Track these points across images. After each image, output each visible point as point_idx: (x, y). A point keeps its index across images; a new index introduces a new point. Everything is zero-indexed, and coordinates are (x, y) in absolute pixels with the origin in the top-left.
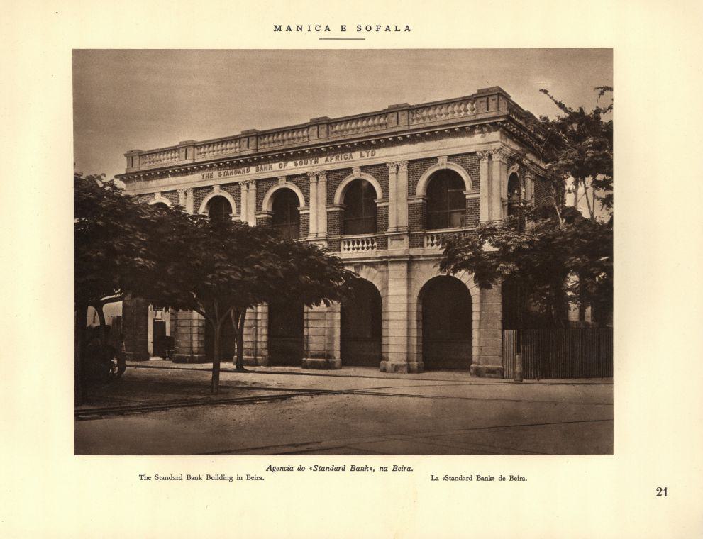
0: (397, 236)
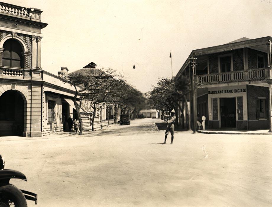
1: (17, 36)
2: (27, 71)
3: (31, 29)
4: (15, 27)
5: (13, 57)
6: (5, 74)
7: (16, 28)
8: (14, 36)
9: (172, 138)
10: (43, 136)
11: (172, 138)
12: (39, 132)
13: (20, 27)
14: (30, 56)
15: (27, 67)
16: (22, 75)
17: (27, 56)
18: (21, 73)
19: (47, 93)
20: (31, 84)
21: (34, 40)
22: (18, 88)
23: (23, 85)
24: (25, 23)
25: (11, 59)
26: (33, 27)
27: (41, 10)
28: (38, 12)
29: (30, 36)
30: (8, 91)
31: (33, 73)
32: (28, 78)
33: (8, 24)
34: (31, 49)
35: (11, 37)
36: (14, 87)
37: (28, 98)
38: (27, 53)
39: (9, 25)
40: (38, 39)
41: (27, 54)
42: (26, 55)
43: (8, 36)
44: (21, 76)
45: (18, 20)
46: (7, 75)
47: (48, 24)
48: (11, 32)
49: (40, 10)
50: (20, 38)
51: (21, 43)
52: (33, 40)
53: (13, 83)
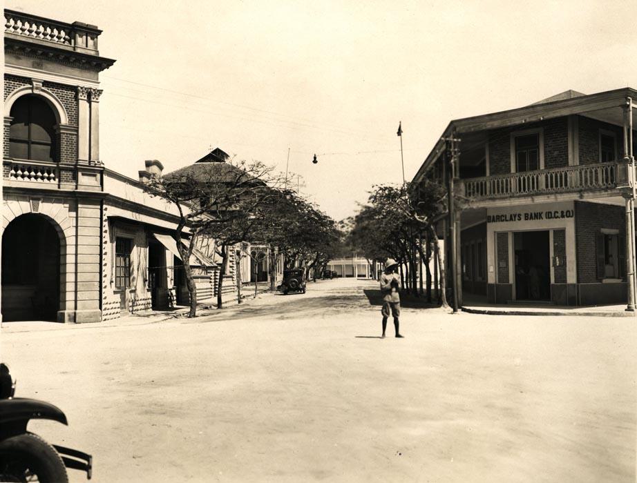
1: (43, 88)
3: (76, 72)
4: (38, 66)
6: (16, 176)
8: (37, 88)
14: (73, 135)
15: (65, 161)
17: (67, 134)
18: (52, 175)
20: (75, 200)
22: (46, 209)
23: (58, 201)
24: (62, 57)
25: (29, 142)
27: (99, 29)
30: (23, 215)
32: (68, 187)
34: (75, 118)
35: (30, 91)
36: (36, 207)
37: (69, 233)
40: (93, 96)
43: (22, 87)
46: (19, 178)
47: (115, 61)
49: (97, 27)
53: (35, 196)
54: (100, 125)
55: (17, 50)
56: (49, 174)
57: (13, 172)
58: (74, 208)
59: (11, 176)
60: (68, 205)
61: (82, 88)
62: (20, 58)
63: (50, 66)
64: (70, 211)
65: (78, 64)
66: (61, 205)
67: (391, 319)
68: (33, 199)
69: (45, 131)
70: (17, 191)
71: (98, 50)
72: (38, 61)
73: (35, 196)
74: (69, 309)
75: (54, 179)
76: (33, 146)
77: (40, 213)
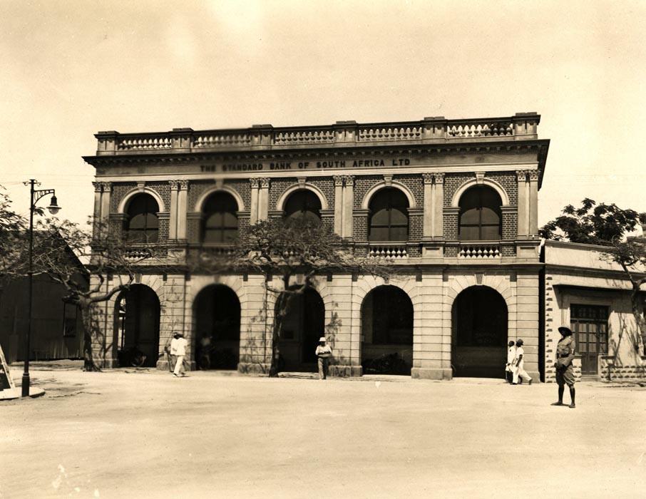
0: (434, 245)
1: (486, 178)
2: (508, 245)
3: (515, 158)
4: (480, 161)
5: (485, 221)
6: (466, 255)
7: (143, 173)
8: (480, 179)
9: (573, 393)
10: (549, 382)
11: (573, 393)
12: (533, 372)
13: (448, 159)
14: (514, 214)
15: (507, 238)
16: (405, 255)
17: (508, 214)
18: (497, 251)
19: (560, 289)
20: (515, 271)
21: (522, 179)
22: (489, 281)
23: (500, 274)
24: (509, 148)
25: (480, 225)
26: (517, 153)
27: (538, 114)
28: (534, 119)
29: (513, 173)
30: (469, 288)
31: (518, 248)
32: (509, 261)
33: (465, 159)
34: (514, 199)
35: (475, 183)
36: (479, 280)
37: (510, 301)
38: (507, 209)
39: (469, 159)
40: (182, 186)
41: (415, 212)
42: (505, 214)
43: (132, 189)
44: (404, 257)
45: (493, 146)
46: (468, 257)
47: (83, 157)
48: (474, 172)
49: (271, 125)
50: (489, 179)
51: (293, 192)
52: (519, 180)
53: (478, 271)
54: (539, 201)
55: (392, 154)
56: (494, 250)
57: (463, 251)
58: (514, 279)
59: (461, 255)
60: (509, 277)
61: (520, 171)
62: (464, 157)
63: (491, 158)
64: (511, 281)
65: (454, 153)
66: (238, 277)
67: (567, 388)
68: (476, 273)
69: (494, 213)
70: (462, 268)
71: (538, 133)
72: (480, 156)
73: (478, 271)
74: (416, 367)
75: (498, 254)
76: (483, 228)
77: (483, 286)
